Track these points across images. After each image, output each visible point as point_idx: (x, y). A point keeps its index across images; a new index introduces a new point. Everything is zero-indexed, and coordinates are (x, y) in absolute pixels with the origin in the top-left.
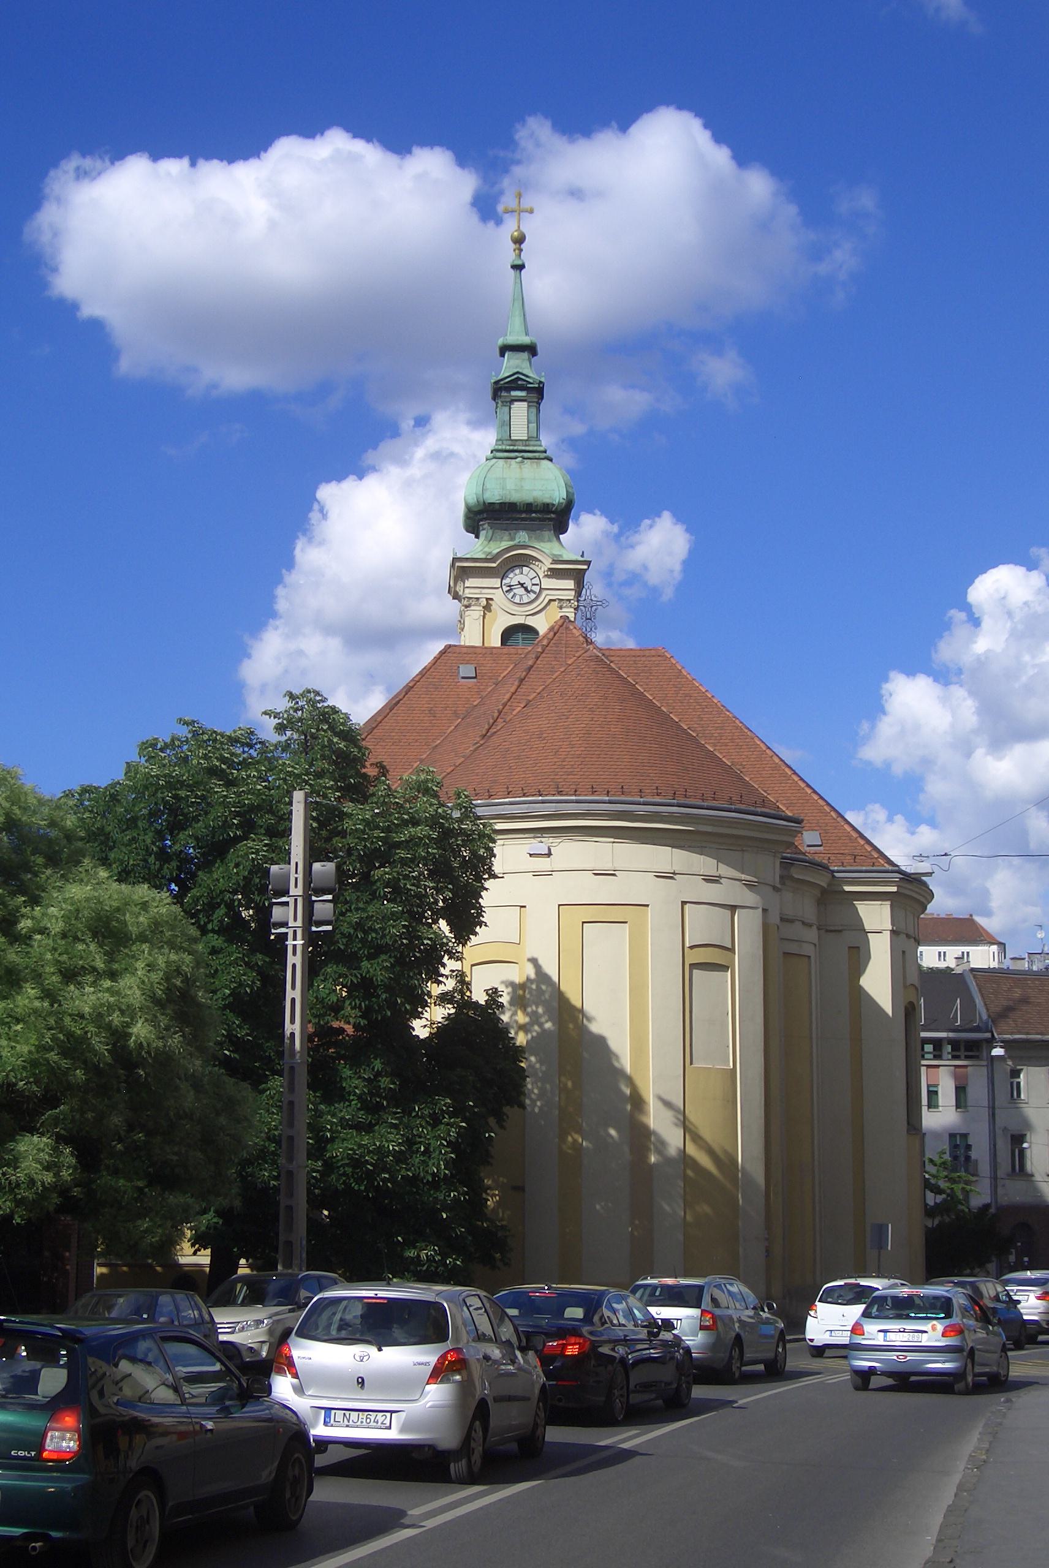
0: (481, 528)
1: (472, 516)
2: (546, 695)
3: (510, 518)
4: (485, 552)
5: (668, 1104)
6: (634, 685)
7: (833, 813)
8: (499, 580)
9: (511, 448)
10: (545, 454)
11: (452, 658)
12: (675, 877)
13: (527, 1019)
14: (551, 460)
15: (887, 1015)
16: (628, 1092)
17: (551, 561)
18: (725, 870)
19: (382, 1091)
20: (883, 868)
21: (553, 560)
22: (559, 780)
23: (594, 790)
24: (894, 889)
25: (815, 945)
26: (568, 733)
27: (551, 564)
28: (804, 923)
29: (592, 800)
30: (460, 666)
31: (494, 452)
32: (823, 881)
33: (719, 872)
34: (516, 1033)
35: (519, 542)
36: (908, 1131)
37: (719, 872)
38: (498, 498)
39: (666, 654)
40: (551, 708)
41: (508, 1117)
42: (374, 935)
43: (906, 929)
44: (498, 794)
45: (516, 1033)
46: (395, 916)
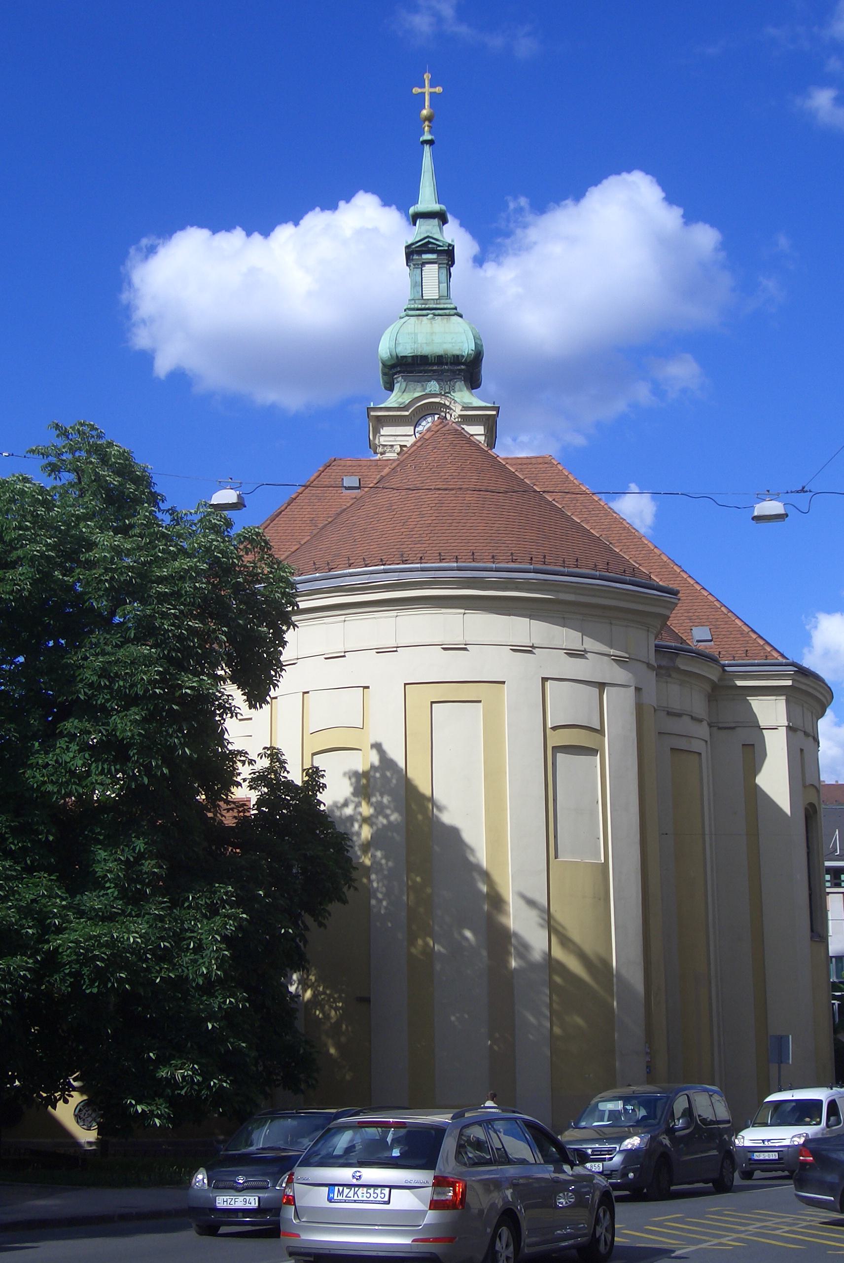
0: (395, 381)
1: (387, 370)
2: (399, 469)
3: (424, 370)
4: (398, 402)
5: (531, 903)
6: (504, 465)
7: (723, 609)
8: (412, 428)
9: (423, 306)
10: (455, 311)
11: (337, 471)
12: (534, 650)
13: (372, 811)
14: (461, 316)
15: (786, 815)
16: (484, 889)
17: (460, 408)
18: (590, 644)
19: (145, 876)
20: (777, 661)
21: (463, 407)
22: (405, 550)
23: (442, 558)
24: (789, 683)
25: (706, 742)
26: (420, 503)
27: (461, 410)
28: (692, 718)
29: (439, 567)
30: (344, 478)
31: (407, 311)
32: (713, 675)
33: (585, 646)
34: (360, 827)
35: (430, 391)
36: (812, 938)
37: (585, 646)
38: (409, 352)
39: (552, 461)
40: (404, 481)
41: (330, 914)
42: (121, 683)
43: (804, 727)
44: (339, 566)
45: (360, 827)
46: (149, 661)
